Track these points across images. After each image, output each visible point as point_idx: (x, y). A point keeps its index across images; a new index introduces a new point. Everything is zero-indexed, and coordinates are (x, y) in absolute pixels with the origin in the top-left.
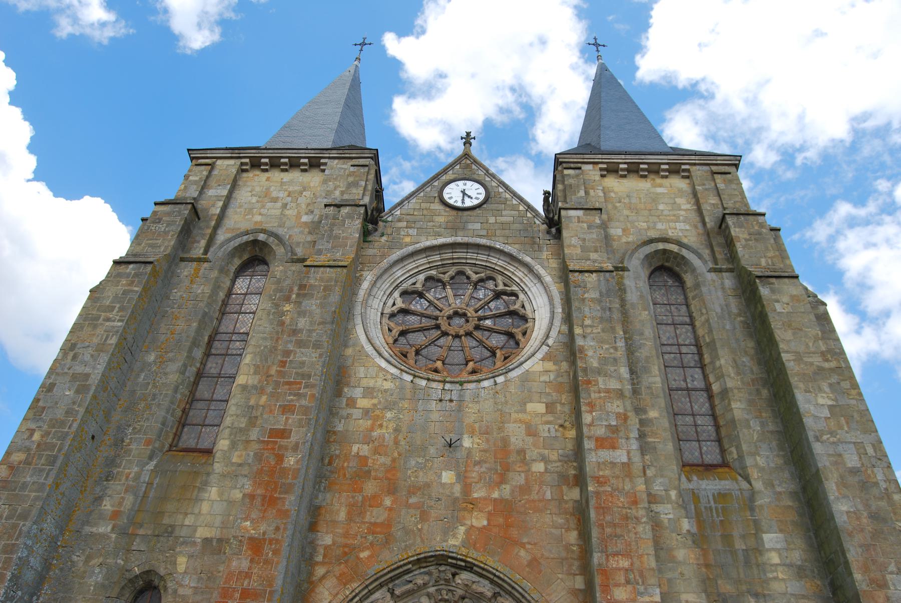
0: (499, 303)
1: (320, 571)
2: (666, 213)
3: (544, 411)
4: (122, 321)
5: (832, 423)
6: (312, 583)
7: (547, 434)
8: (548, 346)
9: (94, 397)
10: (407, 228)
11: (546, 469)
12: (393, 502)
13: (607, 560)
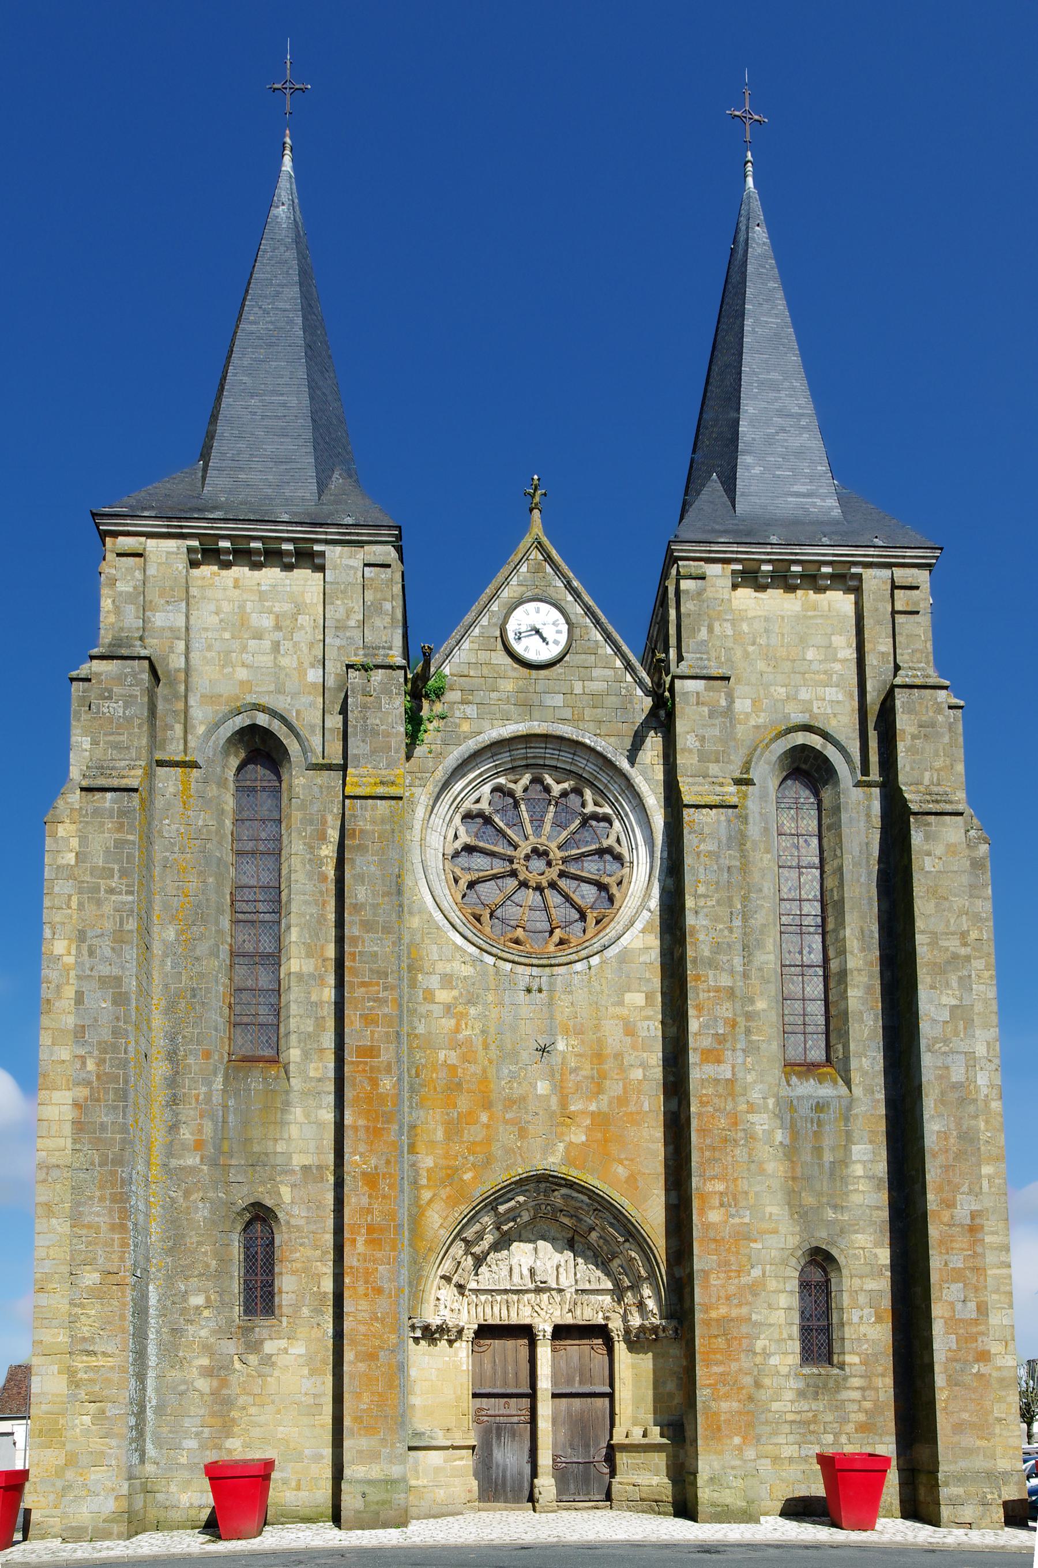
1: (426, 1195)
2: (815, 666)
3: (643, 1003)
4: (131, 893)
5: (949, 1028)
6: (420, 1207)
7: (646, 1034)
8: (650, 911)
10: (462, 703)
11: (645, 1075)
12: (490, 1118)
13: (704, 1184)
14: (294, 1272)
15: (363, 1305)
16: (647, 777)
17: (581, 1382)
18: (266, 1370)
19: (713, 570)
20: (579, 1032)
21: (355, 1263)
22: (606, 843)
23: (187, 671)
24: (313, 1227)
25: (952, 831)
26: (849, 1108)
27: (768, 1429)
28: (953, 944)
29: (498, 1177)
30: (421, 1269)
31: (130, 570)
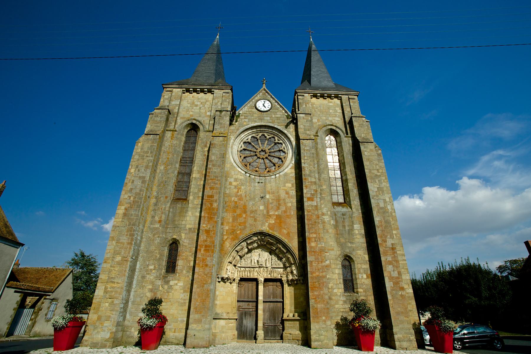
0: (276, 147)
1: (225, 237)
9: (148, 184)
12: (246, 216)
14: (183, 259)
15: (201, 270)
16: (290, 132)
17: (273, 298)
18: (170, 290)
19: (306, 95)
20: (273, 193)
21: (200, 256)
22: (281, 149)
23: (178, 113)
24: (190, 246)
25: (371, 146)
26: (352, 214)
27: (335, 314)
28: (375, 172)
29: (248, 232)
30: (222, 259)
31: (168, 94)
